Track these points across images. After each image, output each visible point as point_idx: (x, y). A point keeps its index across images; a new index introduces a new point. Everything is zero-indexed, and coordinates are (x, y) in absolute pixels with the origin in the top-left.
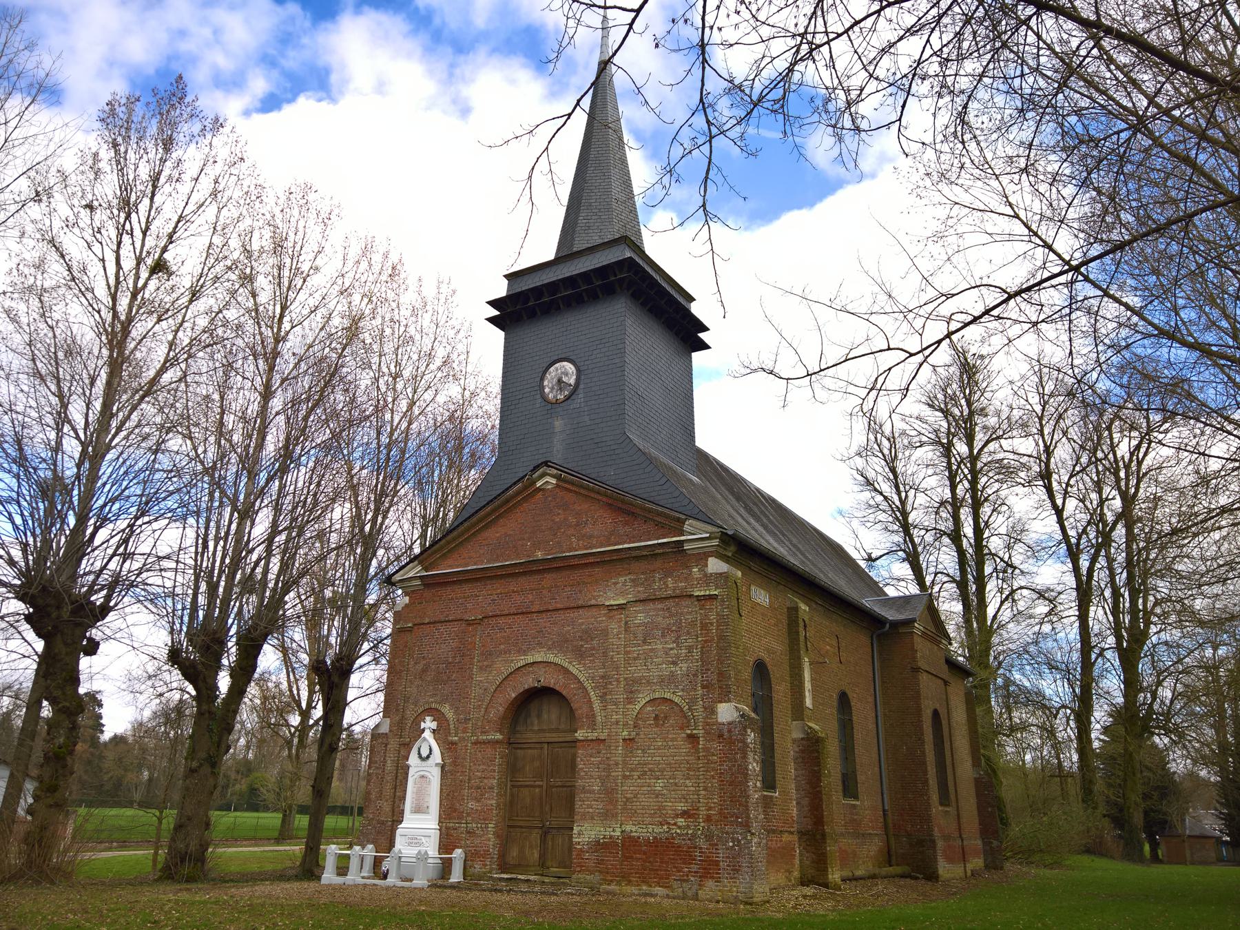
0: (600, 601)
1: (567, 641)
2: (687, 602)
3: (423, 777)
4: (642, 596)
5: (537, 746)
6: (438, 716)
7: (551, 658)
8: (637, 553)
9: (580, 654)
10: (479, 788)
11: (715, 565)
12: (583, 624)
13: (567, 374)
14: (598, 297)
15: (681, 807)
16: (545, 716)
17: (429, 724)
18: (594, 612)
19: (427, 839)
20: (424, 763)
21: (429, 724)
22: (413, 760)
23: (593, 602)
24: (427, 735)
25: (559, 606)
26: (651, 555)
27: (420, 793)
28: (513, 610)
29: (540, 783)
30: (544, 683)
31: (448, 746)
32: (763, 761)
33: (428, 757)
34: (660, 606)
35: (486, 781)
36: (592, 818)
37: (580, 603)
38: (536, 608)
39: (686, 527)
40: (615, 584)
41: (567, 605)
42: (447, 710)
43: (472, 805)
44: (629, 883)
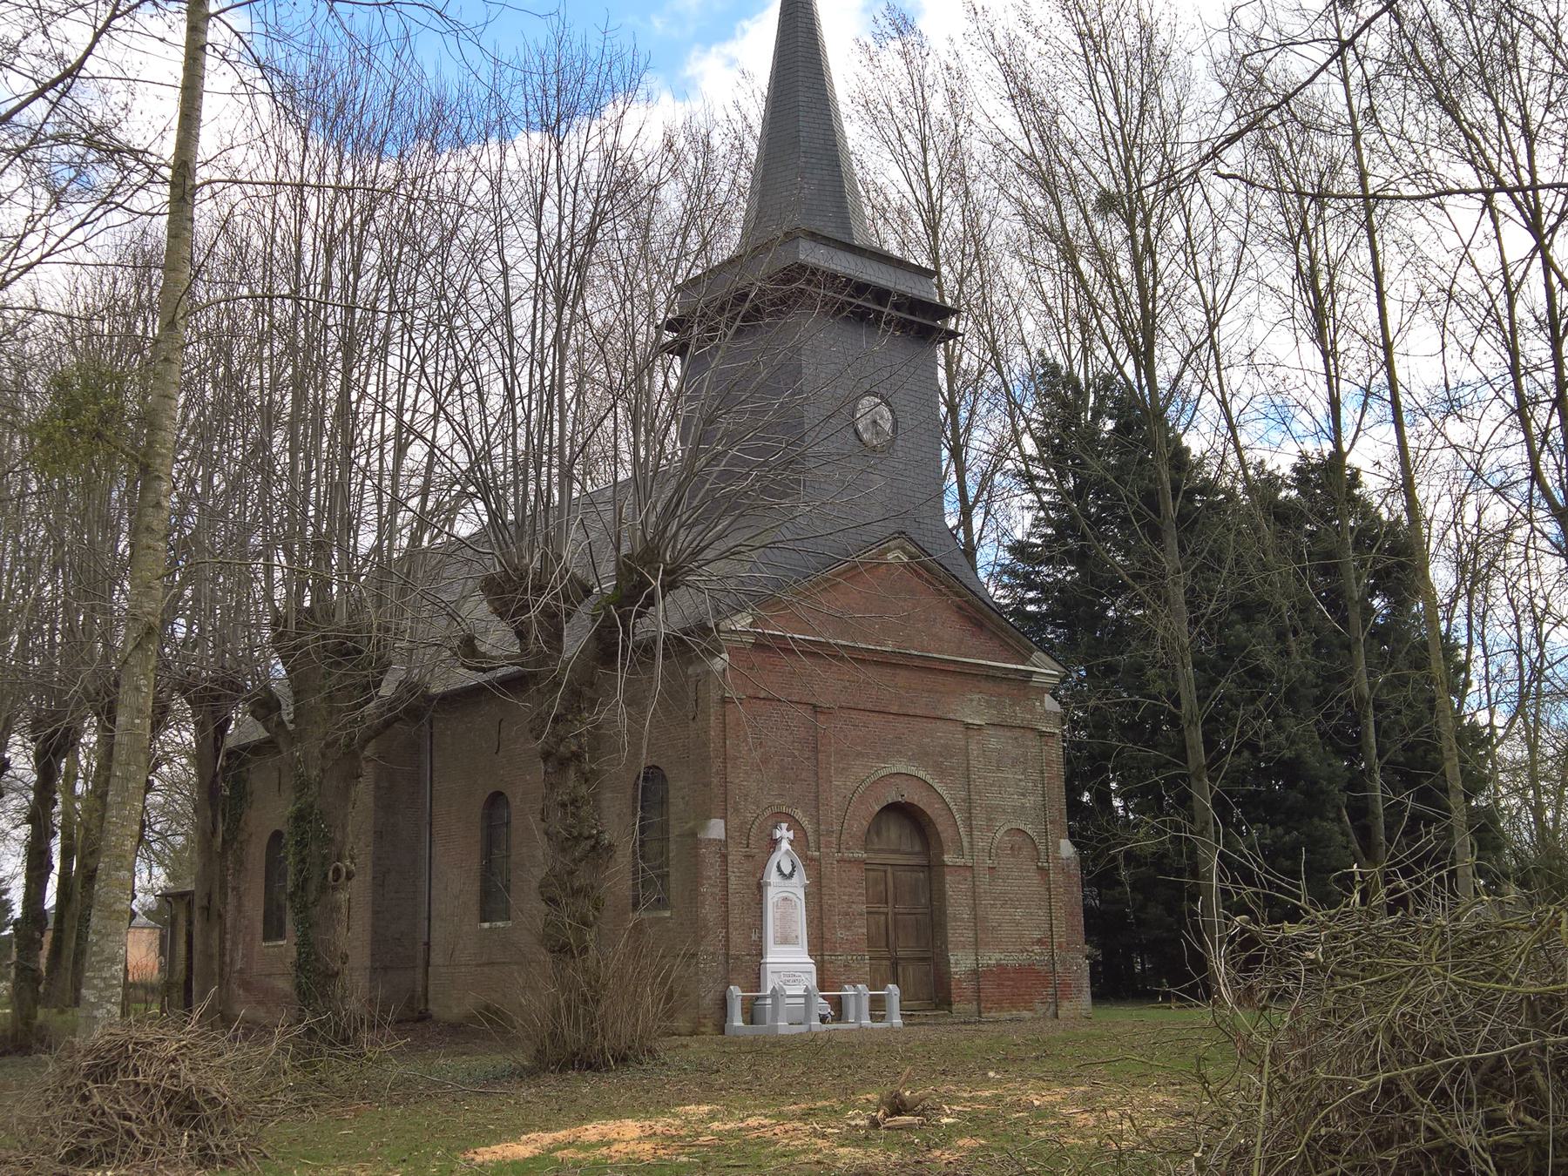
0: (958, 716)
1: (927, 754)
2: (1030, 735)
3: (786, 899)
4: (996, 721)
5: (881, 868)
6: (794, 824)
7: (912, 770)
8: (991, 672)
9: (941, 772)
10: (847, 914)
11: (1051, 704)
12: (941, 738)
13: (882, 418)
14: (1336, 565)
15: (1037, 935)
16: (885, 834)
17: (784, 833)
18: (950, 727)
19: (807, 976)
20: (787, 882)
21: (784, 833)
22: (773, 877)
23: (951, 716)
24: (785, 845)
25: (919, 712)
26: (1003, 677)
27: (785, 919)
28: (869, 706)
29: (885, 910)
30: (907, 798)
31: (813, 866)
32: (38, 757)
33: (791, 875)
34: (1009, 734)
35: (854, 906)
36: (964, 948)
37: (939, 713)
38: (894, 709)
39: (1034, 658)
40: (972, 700)
41: (926, 713)
42: (798, 814)
43: (841, 933)
44: (1002, 1009)
